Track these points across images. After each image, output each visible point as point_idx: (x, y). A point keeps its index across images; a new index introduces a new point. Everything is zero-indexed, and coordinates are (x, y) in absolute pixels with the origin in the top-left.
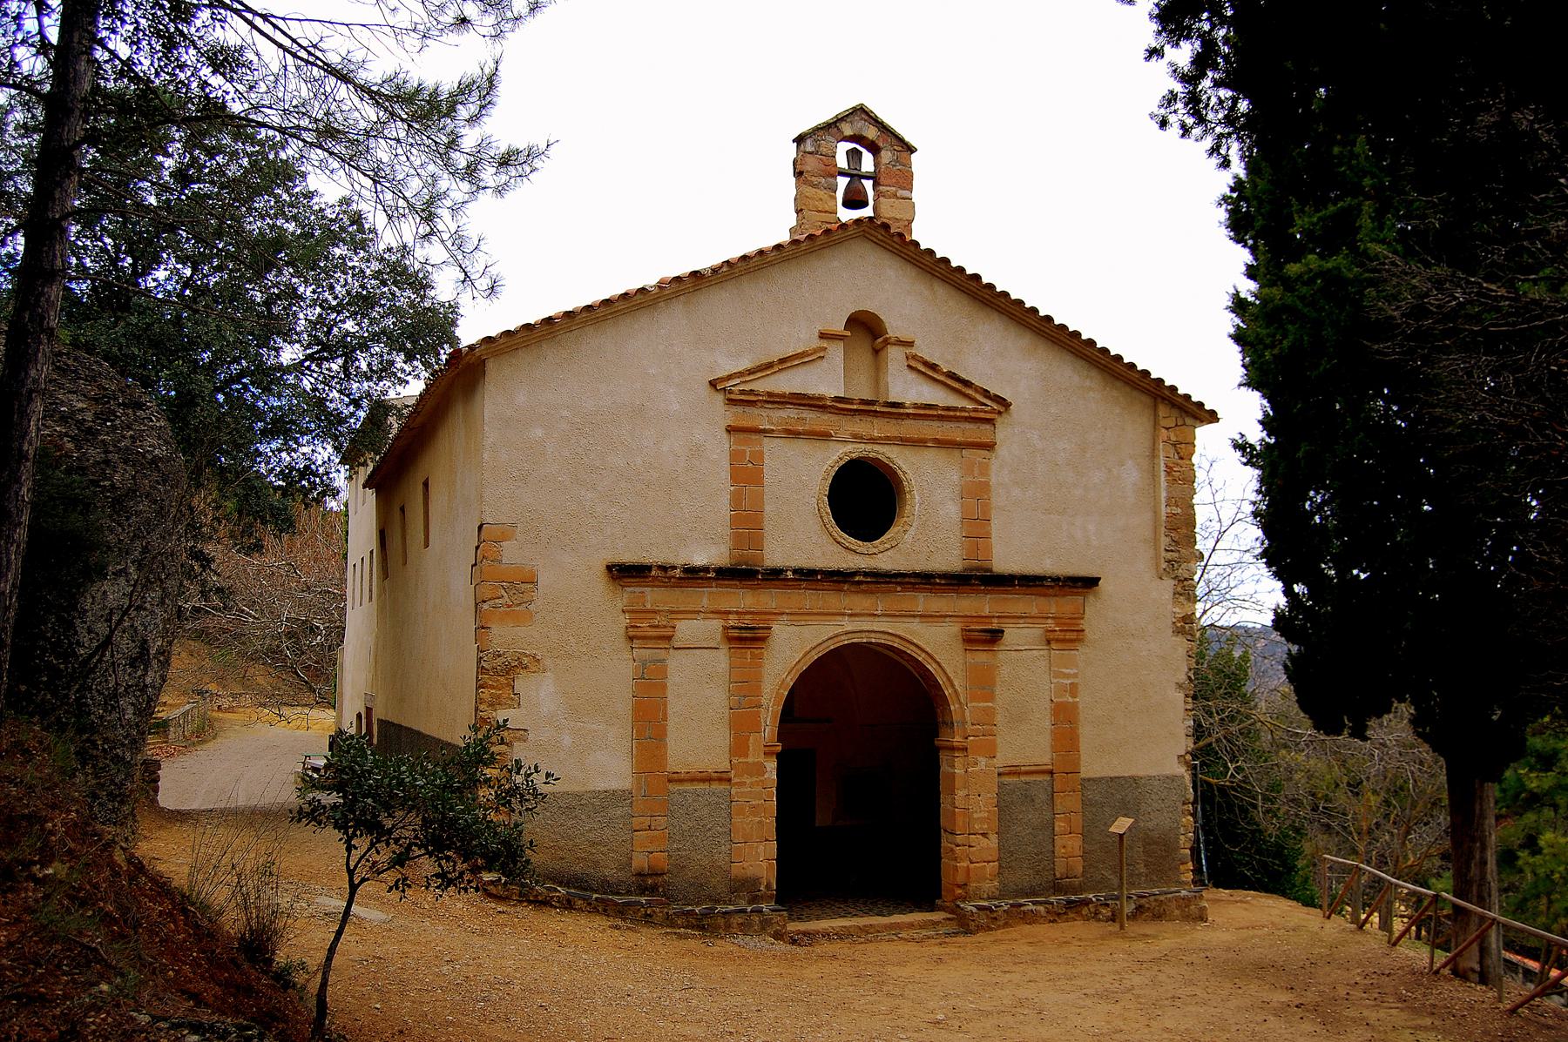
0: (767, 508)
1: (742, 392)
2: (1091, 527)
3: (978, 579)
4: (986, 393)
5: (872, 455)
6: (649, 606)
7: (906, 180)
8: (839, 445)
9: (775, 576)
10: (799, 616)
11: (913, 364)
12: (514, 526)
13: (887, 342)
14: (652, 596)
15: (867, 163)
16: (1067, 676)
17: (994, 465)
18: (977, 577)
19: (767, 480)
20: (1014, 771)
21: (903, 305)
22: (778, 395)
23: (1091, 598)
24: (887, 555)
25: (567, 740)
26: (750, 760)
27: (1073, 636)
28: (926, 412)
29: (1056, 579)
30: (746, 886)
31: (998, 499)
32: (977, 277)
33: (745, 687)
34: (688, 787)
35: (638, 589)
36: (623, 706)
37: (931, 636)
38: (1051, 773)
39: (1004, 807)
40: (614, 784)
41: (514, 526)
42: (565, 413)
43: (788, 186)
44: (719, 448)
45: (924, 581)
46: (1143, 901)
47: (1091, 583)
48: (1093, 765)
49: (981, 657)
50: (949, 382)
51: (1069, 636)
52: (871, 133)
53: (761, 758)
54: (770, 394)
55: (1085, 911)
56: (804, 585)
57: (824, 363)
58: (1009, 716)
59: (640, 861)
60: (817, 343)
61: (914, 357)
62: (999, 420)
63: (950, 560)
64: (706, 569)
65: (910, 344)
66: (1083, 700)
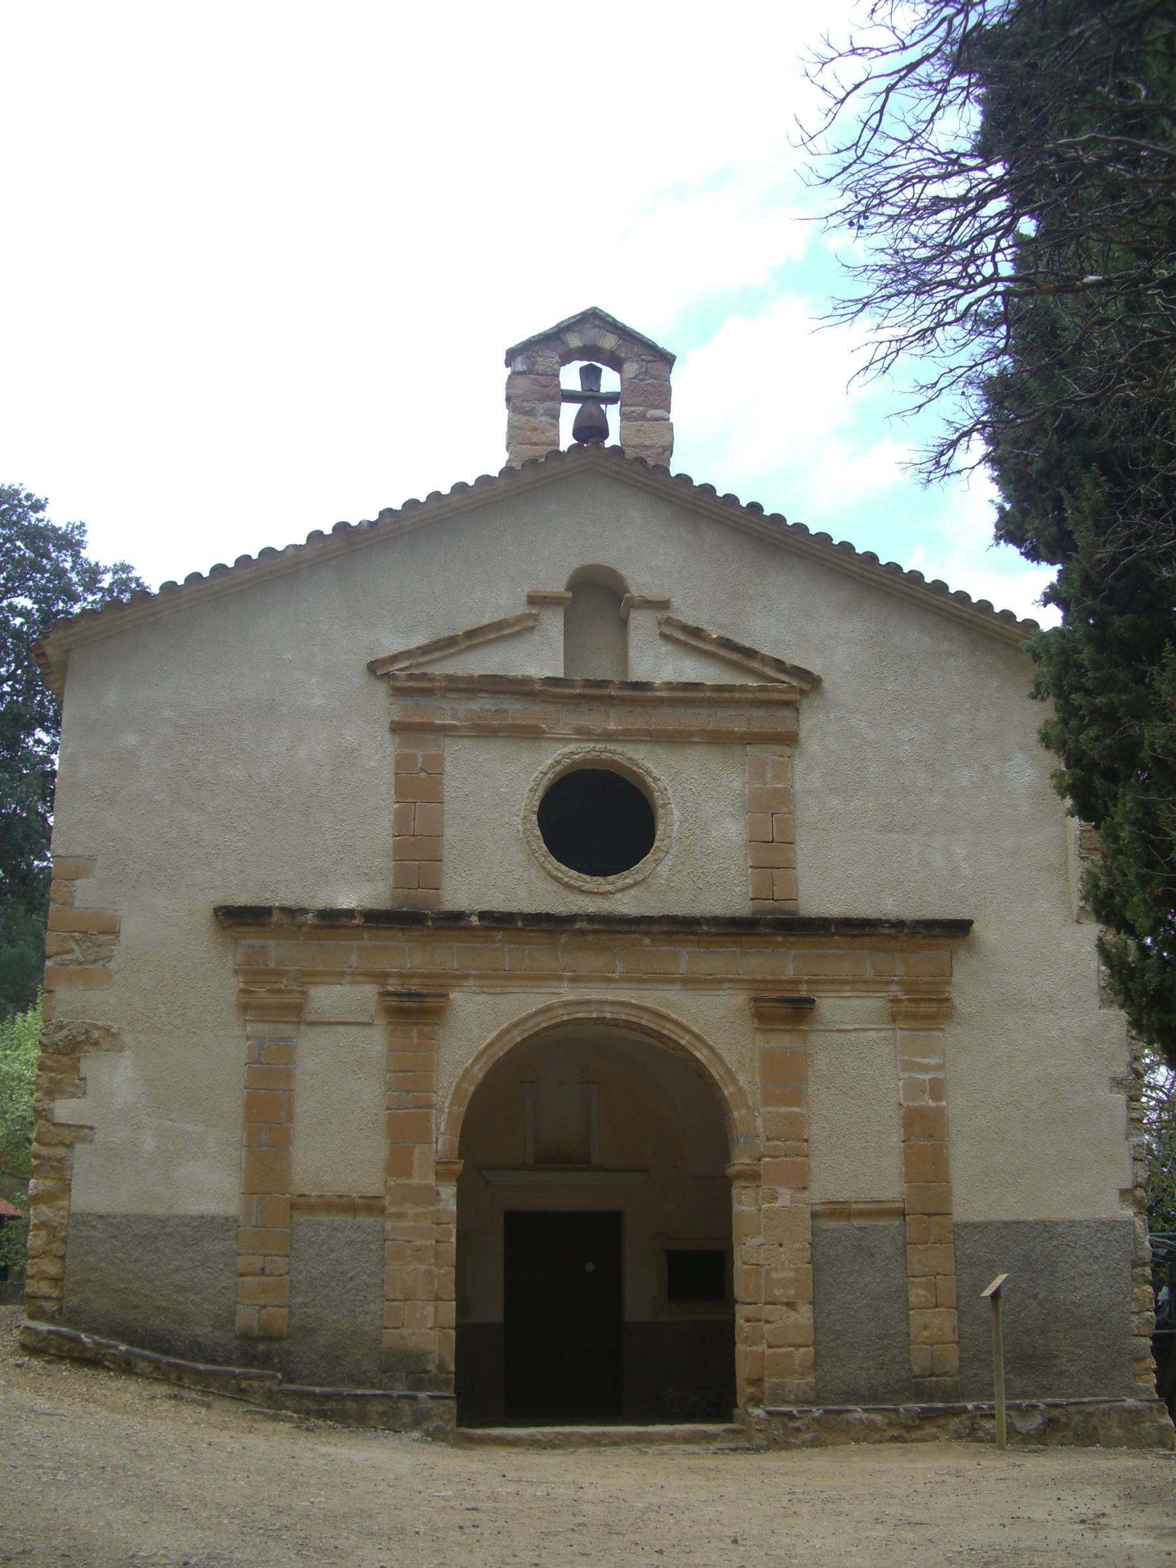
0: (449, 832)
1: (411, 677)
2: (959, 850)
3: (776, 925)
4: (779, 664)
5: (605, 756)
6: (272, 965)
7: (663, 397)
8: (555, 745)
9: (454, 920)
10: (494, 979)
11: (667, 630)
12: (92, 859)
13: (632, 604)
14: (276, 950)
15: (610, 381)
16: (926, 1068)
17: (800, 765)
18: (768, 923)
19: (449, 793)
20: (839, 1210)
21: (651, 558)
22: (462, 679)
23: (963, 954)
24: (625, 895)
25: (149, 1144)
26: (415, 1181)
27: (931, 1008)
28: (686, 694)
29: (899, 924)
30: (408, 1367)
31: (807, 812)
32: (755, 508)
33: (409, 1079)
34: (324, 1218)
35: (258, 942)
36: (231, 1098)
37: (708, 1015)
38: (903, 1214)
39: (820, 1264)
40: (212, 1207)
41: (92, 859)
42: (168, 714)
43: (502, 414)
44: (378, 754)
45: (682, 928)
46: (1056, 1412)
47: (959, 929)
48: (974, 1200)
49: (782, 1041)
50: (723, 653)
51: (923, 1008)
52: (609, 342)
53: (431, 1181)
54: (451, 678)
55: (954, 1423)
56: (499, 935)
57: (535, 637)
58: (826, 1126)
59: (247, 1317)
60: (522, 609)
61: (669, 621)
62: (805, 703)
63: (731, 897)
64: (350, 913)
65: (664, 605)
66: (956, 1105)
